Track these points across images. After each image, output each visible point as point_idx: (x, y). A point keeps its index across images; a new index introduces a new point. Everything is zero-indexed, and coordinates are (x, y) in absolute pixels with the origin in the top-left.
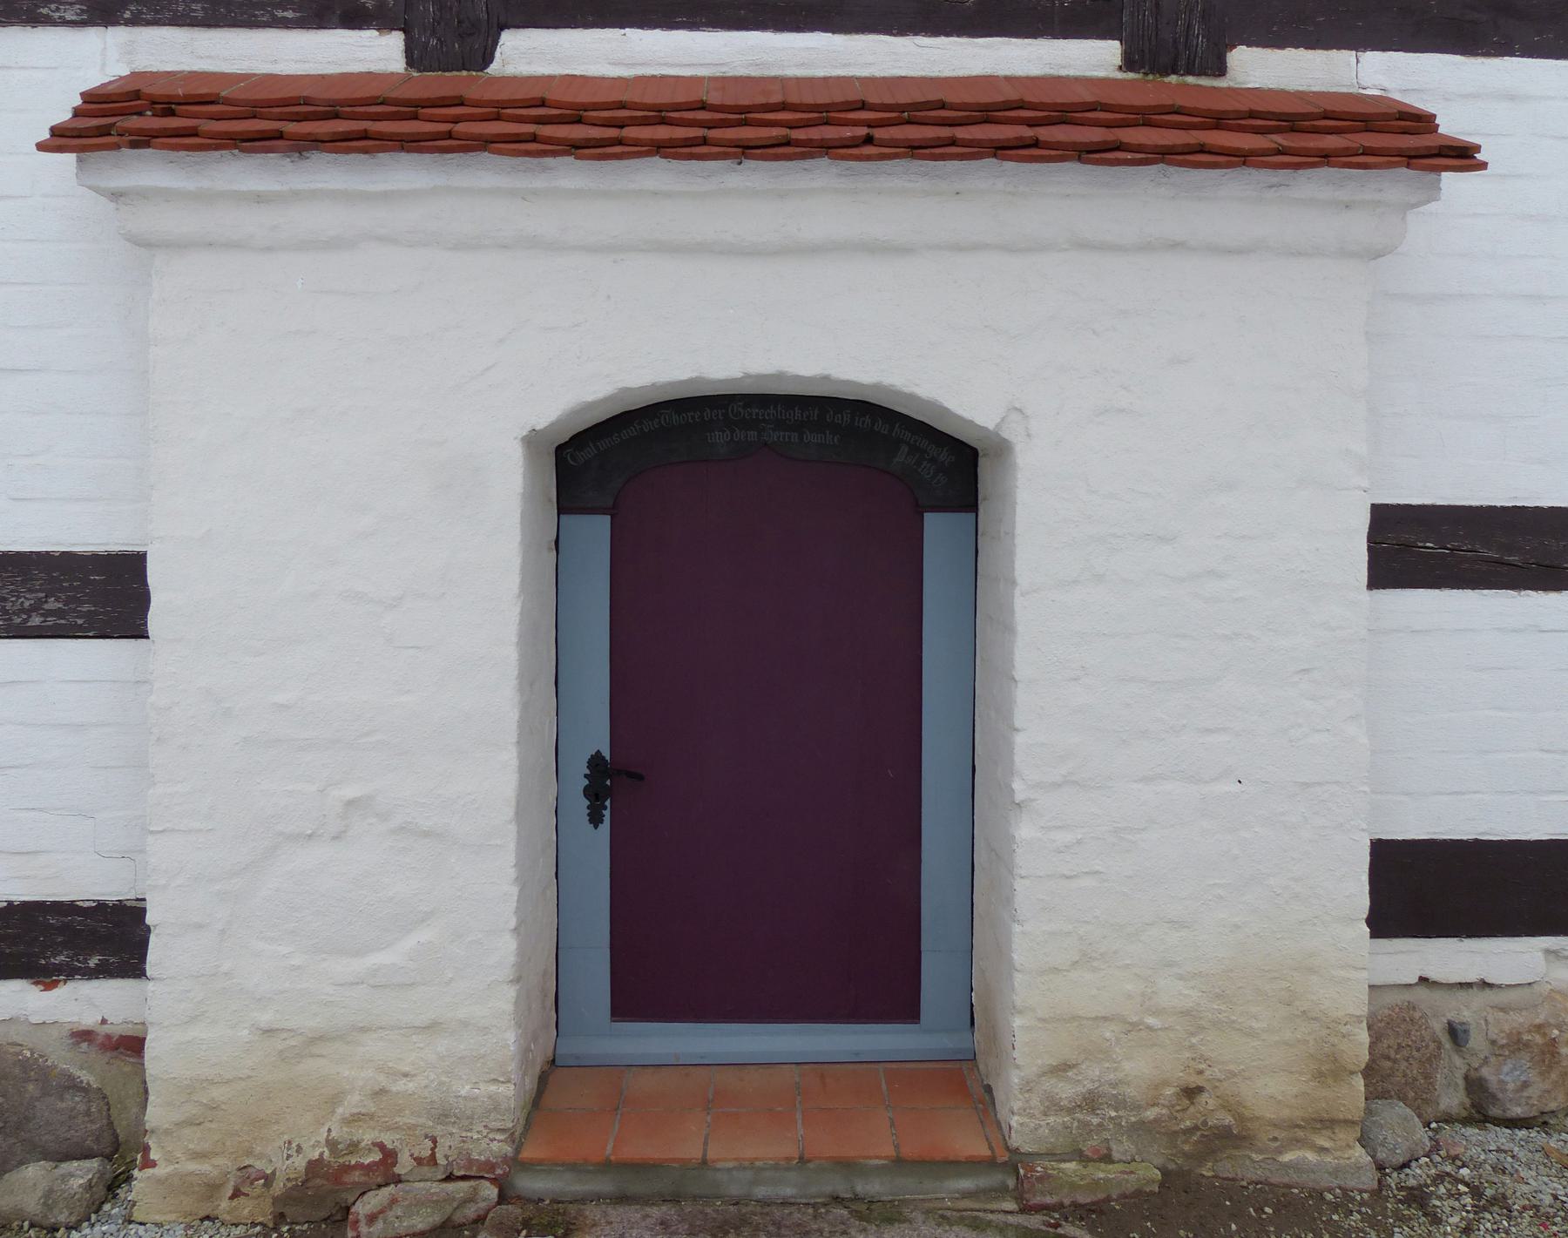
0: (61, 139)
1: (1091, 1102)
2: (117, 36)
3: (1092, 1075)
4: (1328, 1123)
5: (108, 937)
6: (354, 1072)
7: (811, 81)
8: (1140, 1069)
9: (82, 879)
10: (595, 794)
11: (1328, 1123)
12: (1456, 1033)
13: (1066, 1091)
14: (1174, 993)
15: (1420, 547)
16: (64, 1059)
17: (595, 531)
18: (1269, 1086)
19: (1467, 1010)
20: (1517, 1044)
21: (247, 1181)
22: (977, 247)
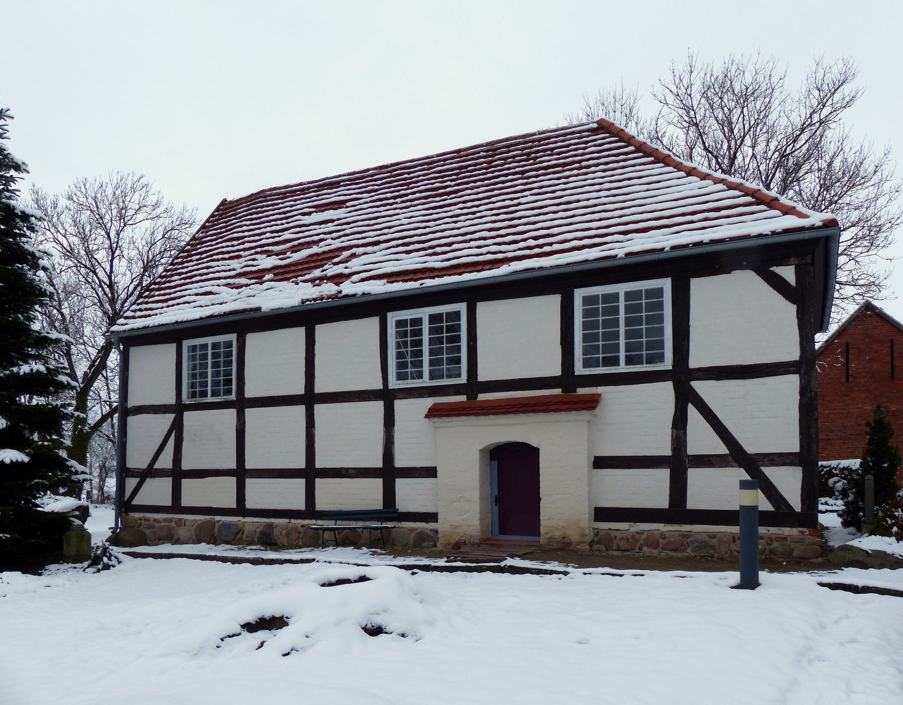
0: (427, 416)
1: (550, 538)
2: (432, 398)
3: (550, 534)
4: (583, 543)
5: (432, 517)
6: (461, 531)
7: (481, 487)
8: (557, 534)
9: (431, 510)
10: (492, 458)
11: (583, 543)
12: (615, 537)
13: (547, 536)
14: (561, 524)
15: (601, 463)
16: (429, 533)
17: (495, 463)
18: (575, 538)
19: (617, 533)
20: (622, 538)
21: (449, 544)
22: (347, 581)
